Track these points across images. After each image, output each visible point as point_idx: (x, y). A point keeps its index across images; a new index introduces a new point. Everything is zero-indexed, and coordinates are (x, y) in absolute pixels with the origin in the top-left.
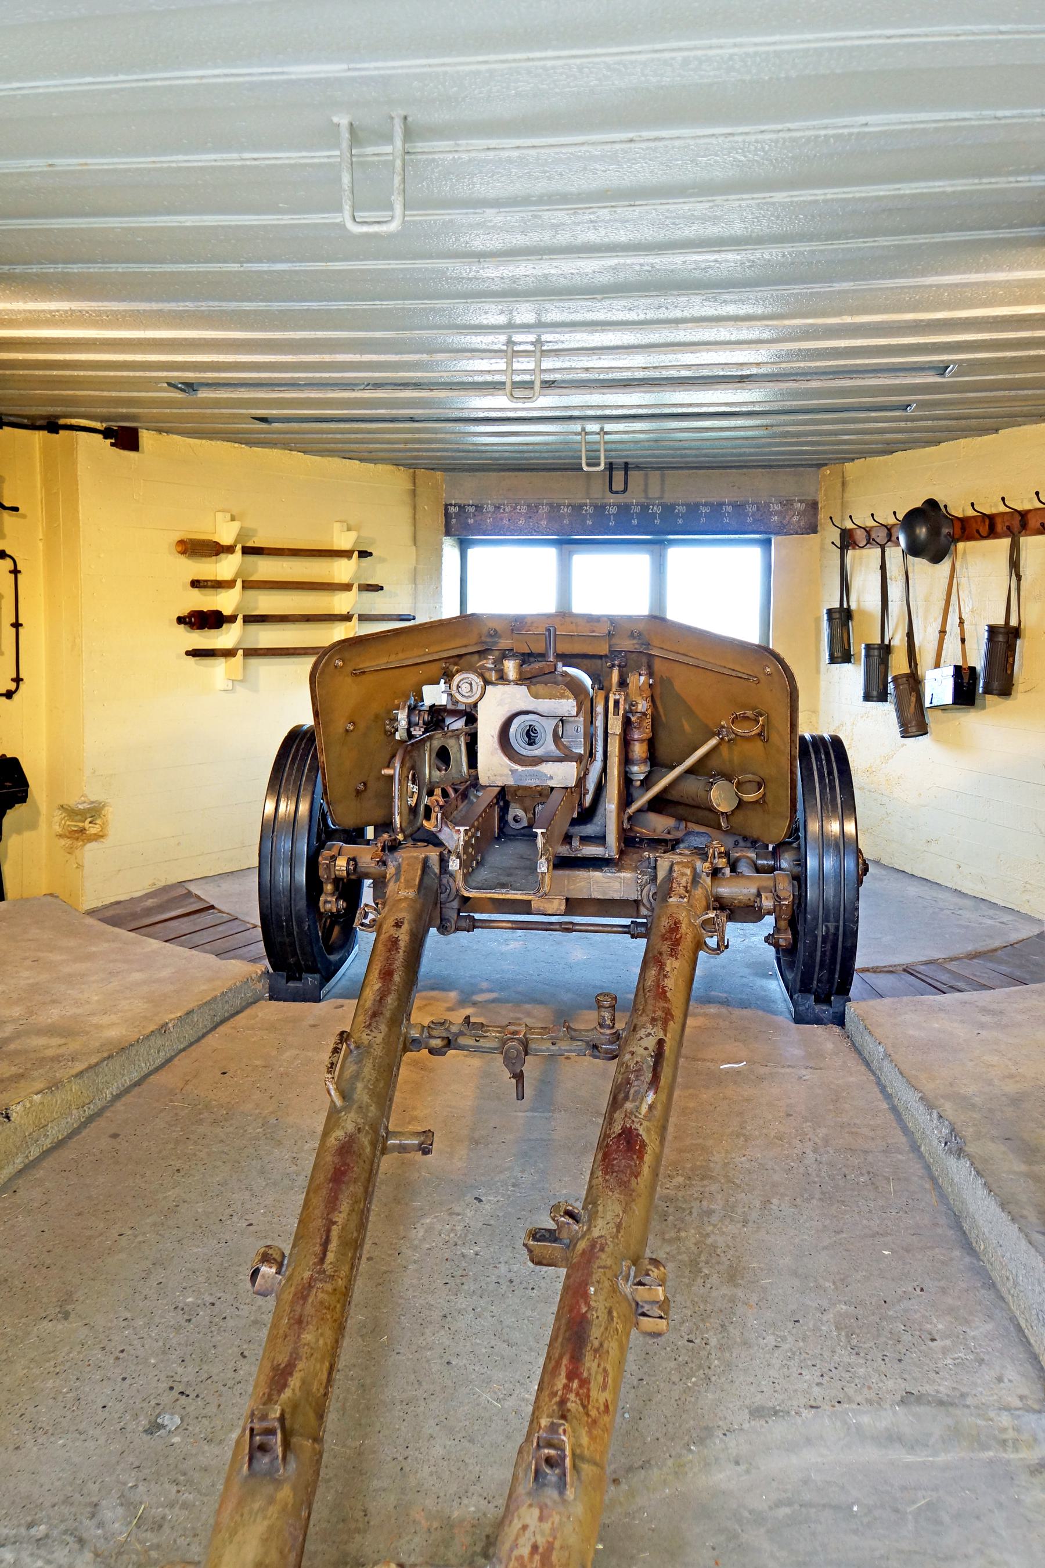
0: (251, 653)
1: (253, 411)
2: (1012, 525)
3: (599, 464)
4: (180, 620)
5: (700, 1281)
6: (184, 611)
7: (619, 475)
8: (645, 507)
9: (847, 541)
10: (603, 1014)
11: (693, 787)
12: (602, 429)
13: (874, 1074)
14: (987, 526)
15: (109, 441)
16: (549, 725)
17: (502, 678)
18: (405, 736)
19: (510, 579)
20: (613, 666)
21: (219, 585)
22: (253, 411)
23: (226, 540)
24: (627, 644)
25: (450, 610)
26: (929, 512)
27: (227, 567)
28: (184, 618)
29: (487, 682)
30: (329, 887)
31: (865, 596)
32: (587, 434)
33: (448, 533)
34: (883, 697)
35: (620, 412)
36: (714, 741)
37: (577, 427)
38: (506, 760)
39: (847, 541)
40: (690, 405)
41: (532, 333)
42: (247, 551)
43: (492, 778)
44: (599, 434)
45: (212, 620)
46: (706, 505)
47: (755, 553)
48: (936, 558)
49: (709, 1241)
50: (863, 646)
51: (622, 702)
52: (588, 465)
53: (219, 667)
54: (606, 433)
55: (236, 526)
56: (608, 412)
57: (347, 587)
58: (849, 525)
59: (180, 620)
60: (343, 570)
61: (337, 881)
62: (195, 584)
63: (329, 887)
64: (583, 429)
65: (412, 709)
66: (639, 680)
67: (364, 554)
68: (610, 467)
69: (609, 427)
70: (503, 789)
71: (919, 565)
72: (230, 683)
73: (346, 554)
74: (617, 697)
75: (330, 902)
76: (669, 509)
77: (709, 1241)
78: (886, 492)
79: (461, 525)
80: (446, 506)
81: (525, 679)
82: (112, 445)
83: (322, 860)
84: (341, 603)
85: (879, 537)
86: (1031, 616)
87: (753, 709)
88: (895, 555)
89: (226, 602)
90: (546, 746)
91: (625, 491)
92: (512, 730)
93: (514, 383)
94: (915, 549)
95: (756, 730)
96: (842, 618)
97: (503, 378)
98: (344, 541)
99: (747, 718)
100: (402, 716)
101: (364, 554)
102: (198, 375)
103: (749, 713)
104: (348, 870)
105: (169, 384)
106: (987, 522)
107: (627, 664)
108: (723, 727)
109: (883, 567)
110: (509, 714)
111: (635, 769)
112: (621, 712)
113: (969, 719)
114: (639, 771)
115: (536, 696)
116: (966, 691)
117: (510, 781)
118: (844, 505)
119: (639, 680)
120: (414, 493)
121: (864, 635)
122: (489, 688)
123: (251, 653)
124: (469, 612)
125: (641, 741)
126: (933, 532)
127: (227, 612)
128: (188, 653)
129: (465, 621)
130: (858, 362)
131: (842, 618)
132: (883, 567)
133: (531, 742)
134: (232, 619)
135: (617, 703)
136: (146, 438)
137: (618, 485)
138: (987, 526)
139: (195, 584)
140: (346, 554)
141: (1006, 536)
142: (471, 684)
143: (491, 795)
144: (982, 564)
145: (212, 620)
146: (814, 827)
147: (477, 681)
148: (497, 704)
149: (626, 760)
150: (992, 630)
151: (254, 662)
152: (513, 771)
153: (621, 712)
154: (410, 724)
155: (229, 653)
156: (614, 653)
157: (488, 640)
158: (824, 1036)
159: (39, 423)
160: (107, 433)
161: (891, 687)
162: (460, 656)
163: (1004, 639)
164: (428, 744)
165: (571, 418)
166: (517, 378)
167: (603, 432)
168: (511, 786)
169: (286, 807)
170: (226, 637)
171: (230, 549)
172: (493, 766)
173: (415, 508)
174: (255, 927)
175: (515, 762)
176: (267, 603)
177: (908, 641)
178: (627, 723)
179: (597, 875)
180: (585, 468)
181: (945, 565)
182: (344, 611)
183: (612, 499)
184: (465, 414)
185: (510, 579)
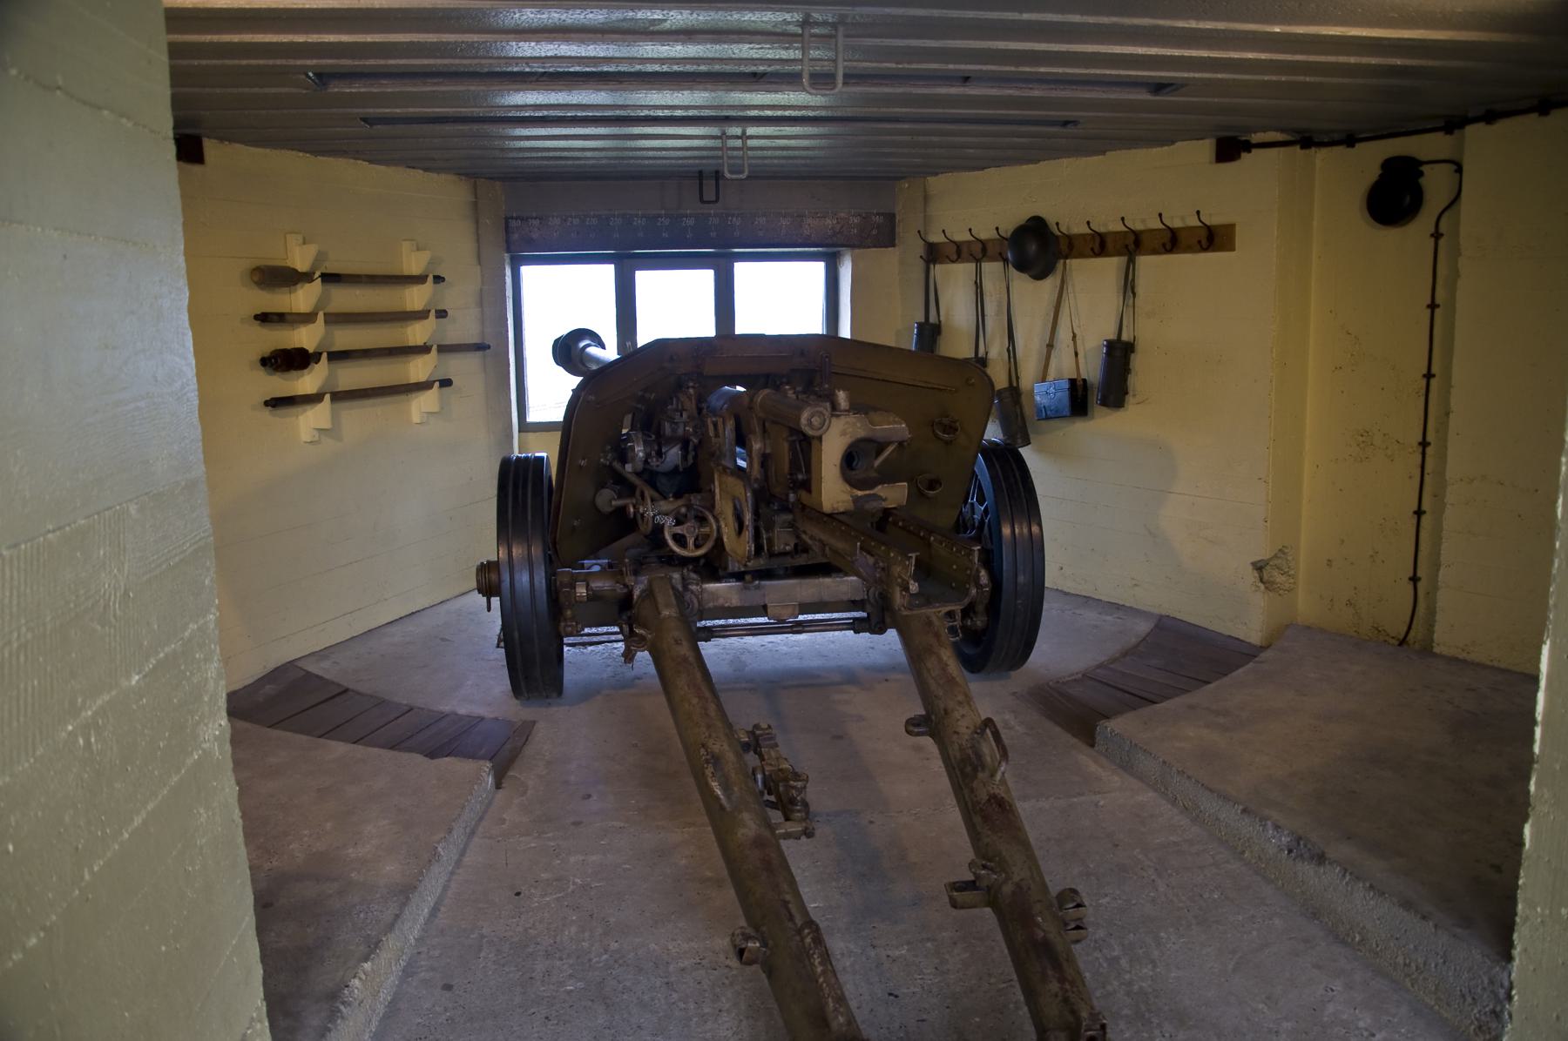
2: (1131, 245)
3: (741, 172)
5: (1157, 1032)
7: (709, 186)
14: (1100, 245)
23: (301, 265)
26: (1035, 228)
27: (303, 298)
28: (269, 358)
37: (737, 131)
39: (934, 254)
41: (797, 10)
42: (330, 278)
45: (295, 360)
48: (1040, 276)
49: (1136, 988)
52: (731, 172)
60: (415, 298)
69: (751, 131)
71: (1022, 284)
77: (1136, 988)
78: (985, 204)
80: (507, 219)
84: (417, 333)
85: (976, 252)
86: (1144, 332)
89: (306, 337)
91: (717, 201)
94: (1022, 266)
106: (1098, 240)
113: (1080, 429)
116: (1079, 400)
118: (927, 220)
120: (475, 205)
123: (338, 397)
126: (1037, 248)
130: (1093, 71)
136: (210, 147)
138: (1100, 245)
139: (264, 318)
141: (1119, 254)
145: (295, 360)
150: (920, 325)
159: (1336, 137)
163: (1119, 354)
167: (744, 137)
170: (307, 382)
171: (307, 277)
173: (477, 222)
176: (347, 338)
181: (1049, 285)
182: (420, 342)
183: (711, 210)
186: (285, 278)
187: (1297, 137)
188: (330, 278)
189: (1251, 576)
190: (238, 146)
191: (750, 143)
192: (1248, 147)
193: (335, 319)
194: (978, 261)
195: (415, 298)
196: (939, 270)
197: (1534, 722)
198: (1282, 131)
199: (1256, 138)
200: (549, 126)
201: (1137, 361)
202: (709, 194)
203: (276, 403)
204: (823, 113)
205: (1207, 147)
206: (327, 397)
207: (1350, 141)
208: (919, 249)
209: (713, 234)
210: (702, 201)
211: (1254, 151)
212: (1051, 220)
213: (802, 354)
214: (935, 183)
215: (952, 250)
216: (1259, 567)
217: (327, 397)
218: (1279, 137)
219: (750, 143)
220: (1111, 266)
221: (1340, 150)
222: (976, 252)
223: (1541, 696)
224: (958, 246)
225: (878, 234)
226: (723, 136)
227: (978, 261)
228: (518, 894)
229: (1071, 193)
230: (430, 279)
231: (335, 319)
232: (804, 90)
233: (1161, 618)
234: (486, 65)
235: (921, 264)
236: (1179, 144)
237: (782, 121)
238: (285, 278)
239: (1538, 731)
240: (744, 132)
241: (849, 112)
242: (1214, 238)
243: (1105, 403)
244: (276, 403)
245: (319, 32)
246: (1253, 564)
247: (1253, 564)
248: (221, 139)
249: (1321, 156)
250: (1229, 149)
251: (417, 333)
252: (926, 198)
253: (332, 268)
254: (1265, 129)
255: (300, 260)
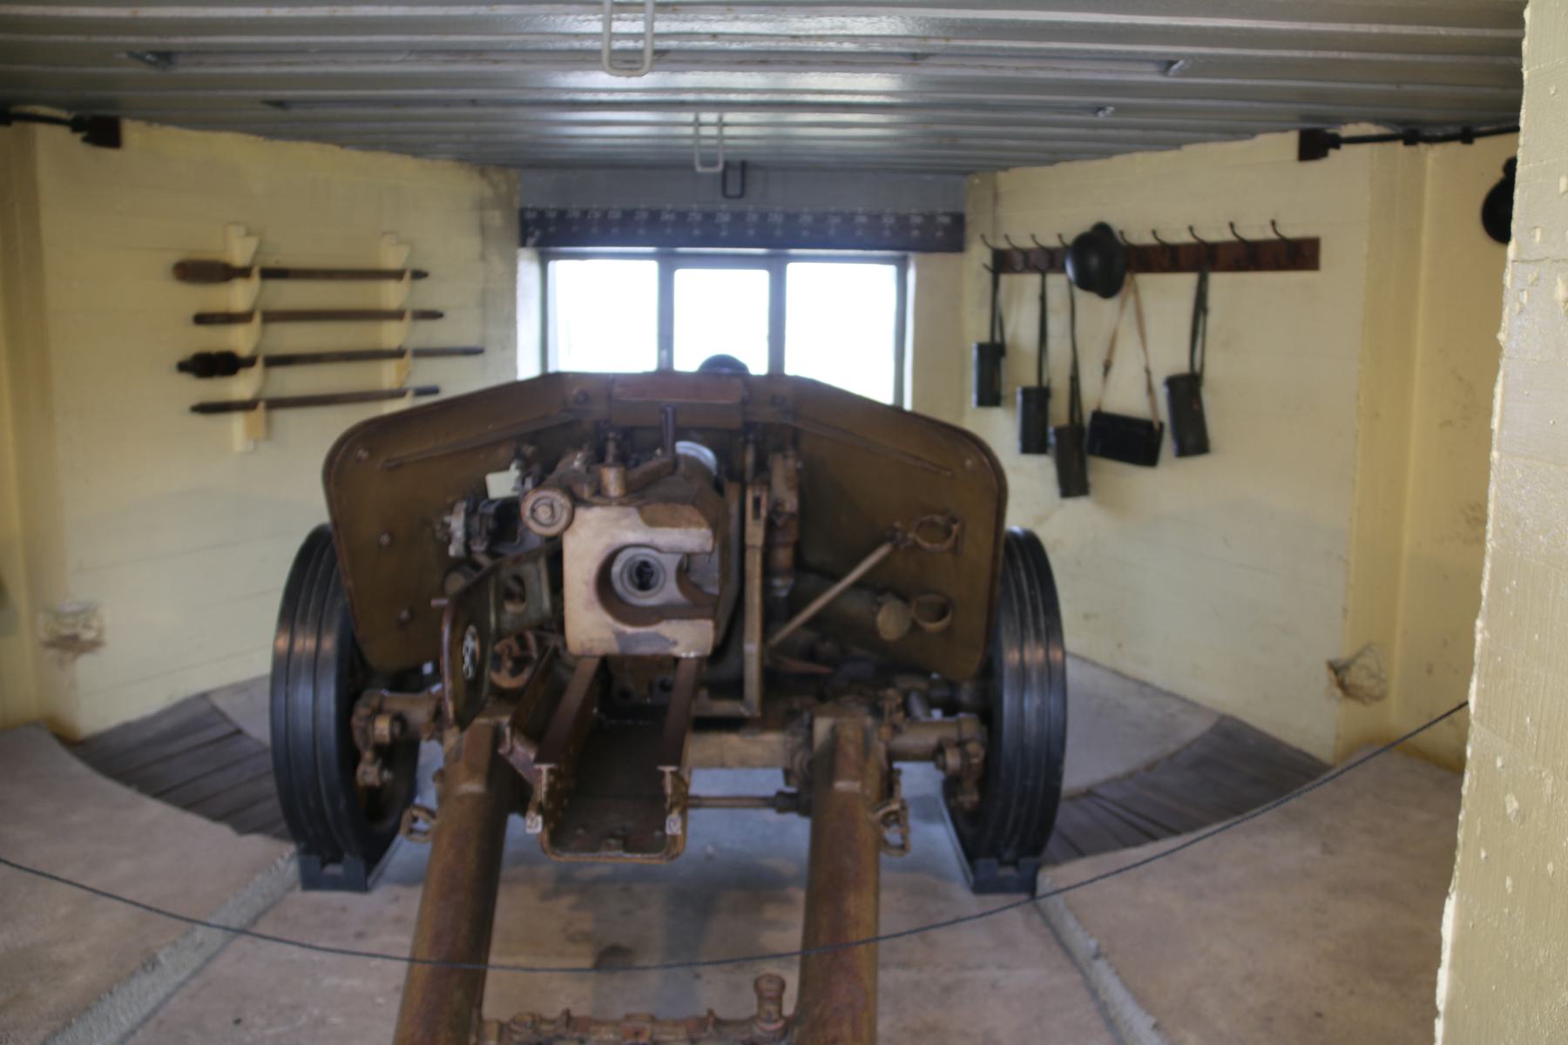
0: (276, 404)
8: (764, 217)
9: (1003, 262)
11: (857, 606)
13: (1081, 971)
14: (1165, 258)
17: (599, 490)
20: (747, 442)
25: (527, 368)
27: (239, 295)
29: (577, 501)
30: (368, 755)
31: (1021, 328)
32: (701, 125)
36: (883, 551)
37: (688, 117)
39: (1003, 262)
42: (269, 274)
46: (835, 214)
47: (890, 271)
50: (1019, 390)
51: (764, 501)
53: (237, 423)
54: (726, 125)
56: (733, 97)
58: (1003, 245)
60: (392, 294)
63: (368, 755)
65: (470, 514)
67: (419, 275)
68: (727, 165)
69: (729, 117)
73: (397, 275)
75: (369, 773)
76: (791, 218)
78: (1052, 207)
79: (554, 230)
83: (356, 722)
84: (391, 335)
85: (1045, 261)
88: (1058, 284)
89: (240, 340)
90: (668, 591)
93: (613, 52)
96: (992, 355)
97: (597, 45)
99: (933, 524)
100: (457, 523)
103: (938, 519)
109: (1043, 299)
110: (610, 550)
111: (778, 582)
112: (763, 512)
114: (782, 586)
115: (652, 522)
117: (614, 648)
119: (783, 469)
121: (1020, 373)
123: (276, 404)
126: (1105, 262)
129: (550, 382)
131: (992, 355)
132: (1043, 299)
134: (250, 362)
135: (757, 502)
137: (733, 189)
138: (1165, 258)
140: (397, 275)
142: (552, 507)
144: (1165, 296)
146: (1011, 657)
147: (561, 501)
148: (593, 536)
149: (768, 572)
152: (620, 635)
153: (763, 512)
154: (469, 536)
155: (247, 406)
156: (749, 426)
158: (1014, 918)
159: (1452, 130)
163: (1186, 391)
164: (493, 580)
166: (617, 45)
167: (721, 124)
169: (306, 643)
170: (241, 386)
171: (244, 273)
172: (588, 627)
178: (770, 527)
180: (699, 169)
184: (544, 96)
186: (223, 273)
187: (1400, 130)
188: (269, 274)
189: (1325, 677)
191: (728, 131)
192: (1336, 142)
193: (271, 317)
194: (1043, 273)
195: (392, 294)
197: (1436, 1013)
198: (1376, 121)
199: (1347, 131)
200: (611, 106)
201: (1210, 399)
202: (733, 189)
203: (205, 409)
206: (262, 405)
207: (1467, 136)
208: (986, 257)
210: (725, 195)
211: (1345, 148)
212: (1116, 222)
213: (609, 397)
214: (1006, 180)
215: (1018, 258)
216: (1338, 670)
217: (262, 405)
220: (1185, 283)
221: (1455, 147)
222: (1045, 261)
223: (1443, 975)
224: (1025, 253)
225: (945, 236)
227: (1043, 273)
231: (271, 317)
233: (1224, 719)
234: (532, 42)
235: (987, 277)
236: (1261, 139)
237: (852, 103)
238: (223, 273)
239: (1439, 1026)
241: (917, 99)
242: (1297, 254)
244: (205, 409)
248: (150, 120)
250: (1315, 145)
251: (391, 335)
252: (996, 196)
253: (271, 262)
255: (239, 252)
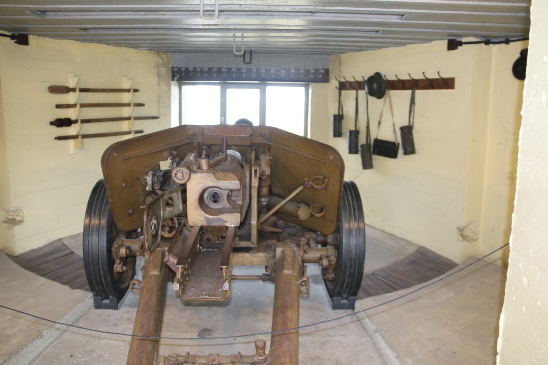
0: (85, 136)
1: (78, 26)
4: (52, 123)
6: (53, 119)
9: (343, 86)
10: (260, 351)
11: (291, 208)
12: (243, 35)
15: (13, 41)
16: (225, 194)
18: (151, 189)
19: (199, 106)
20: (252, 150)
21: (68, 106)
22: (78, 26)
23: (71, 86)
24: (259, 140)
27: (71, 98)
29: (191, 171)
30: (118, 261)
31: (349, 110)
33: (173, 80)
34: (356, 152)
35: (253, 27)
37: (231, 34)
38: (204, 213)
39: (343, 86)
40: (285, 25)
42: (82, 90)
43: (195, 222)
44: (241, 37)
51: (258, 171)
55: (76, 79)
56: (247, 27)
57: (128, 105)
58: (343, 80)
59: (52, 123)
60: (126, 98)
61: (122, 259)
62: (58, 106)
64: (234, 35)
66: (265, 159)
67: (136, 91)
69: (246, 34)
70: (201, 228)
71: (373, 100)
72: (76, 150)
73: (128, 91)
74: (256, 168)
75: (118, 267)
78: (360, 67)
81: (212, 167)
82: (16, 42)
85: (357, 86)
87: (322, 175)
88: (362, 94)
89: (71, 114)
90: (224, 203)
92: (205, 195)
94: (372, 93)
95: (324, 186)
96: (339, 119)
98: (126, 85)
101: (136, 91)
102: (35, 6)
104: (126, 253)
105: (31, 11)
107: (257, 145)
108: (305, 181)
109: (357, 99)
110: (203, 189)
111: (263, 199)
115: (218, 179)
117: (205, 223)
118: (340, 72)
119: (265, 159)
121: (348, 125)
122: (193, 175)
123: (85, 136)
124: (183, 124)
125: (266, 186)
126: (378, 86)
127: (73, 118)
128: (56, 138)
131: (339, 119)
132: (357, 99)
133: (215, 202)
135: (256, 171)
136: (32, 39)
139: (58, 106)
140: (128, 91)
142: (183, 173)
143: (196, 230)
148: (197, 183)
151: (86, 140)
152: (207, 219)
153: (258, 175)
154: (153, 183)
156: (253, 144)
157: (191, 137)
159: (502, 39)
160: (12, 37)
161: (360, 149)
162: (178, 147)
163: (407, 132)
165: (229, 29)
167: (243, 37)
168: (205, 226)
170: (72, 130)
172: (196, 217)
174: (83, 276)
175: (209, 214)
177: (367, 130)
178: (260, 179)
179: (247, 255)
185: (199, 106)
187: (483, 40)
190: (46, 38)
191: (245, 39)
192: (461, 44)
193: (83, 106)
195: (126, 98)
196: (343, 92)
198: (475, 36)
199: (464, 40)
202: (247, 60)
204: (300, 28)
205: (445, 43)
207: (507, 42)
209: (254, 76)
211: (464, 45)
212: (383, 73)
215: (348, 85)
218: (474, 39)
219: (245, 39)
221: (503, 45)
222: (357, 86)
224: (350, 83)
226: (234, 36)
228: (71, 356)
229: (396, 63)
230: (132, 91)
231: (83, 106)
232: (201, 18)
235: (337, 91)
236: (434, 42)
238: (67, 90)
240: (234, 35)
242: (447, 84)
243: (406, 153)
245: (474, 5)
246: (458, 228)
247: (458, 228)
249: (494, 48)
250: (453, 45)
252: (340, 63)
253: (83, 87)
254: (468, 35)
